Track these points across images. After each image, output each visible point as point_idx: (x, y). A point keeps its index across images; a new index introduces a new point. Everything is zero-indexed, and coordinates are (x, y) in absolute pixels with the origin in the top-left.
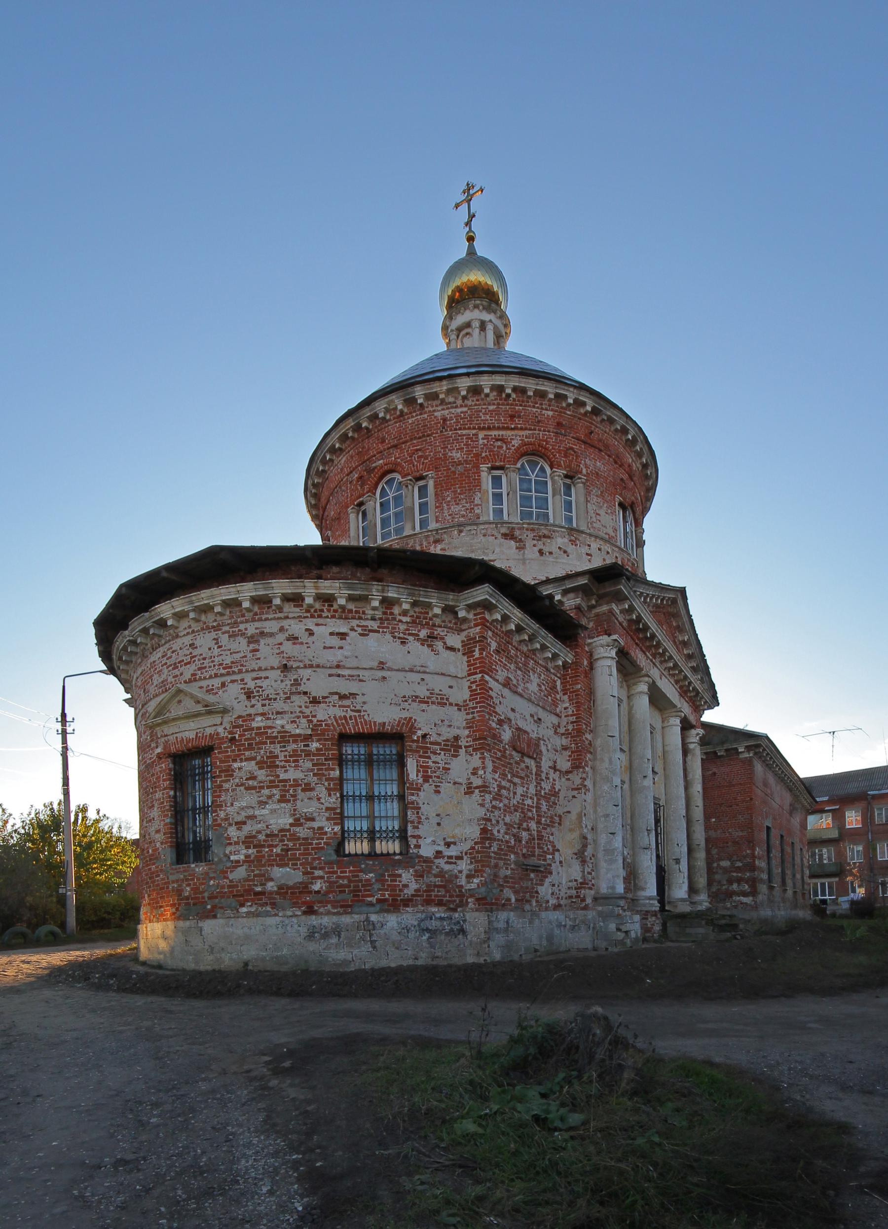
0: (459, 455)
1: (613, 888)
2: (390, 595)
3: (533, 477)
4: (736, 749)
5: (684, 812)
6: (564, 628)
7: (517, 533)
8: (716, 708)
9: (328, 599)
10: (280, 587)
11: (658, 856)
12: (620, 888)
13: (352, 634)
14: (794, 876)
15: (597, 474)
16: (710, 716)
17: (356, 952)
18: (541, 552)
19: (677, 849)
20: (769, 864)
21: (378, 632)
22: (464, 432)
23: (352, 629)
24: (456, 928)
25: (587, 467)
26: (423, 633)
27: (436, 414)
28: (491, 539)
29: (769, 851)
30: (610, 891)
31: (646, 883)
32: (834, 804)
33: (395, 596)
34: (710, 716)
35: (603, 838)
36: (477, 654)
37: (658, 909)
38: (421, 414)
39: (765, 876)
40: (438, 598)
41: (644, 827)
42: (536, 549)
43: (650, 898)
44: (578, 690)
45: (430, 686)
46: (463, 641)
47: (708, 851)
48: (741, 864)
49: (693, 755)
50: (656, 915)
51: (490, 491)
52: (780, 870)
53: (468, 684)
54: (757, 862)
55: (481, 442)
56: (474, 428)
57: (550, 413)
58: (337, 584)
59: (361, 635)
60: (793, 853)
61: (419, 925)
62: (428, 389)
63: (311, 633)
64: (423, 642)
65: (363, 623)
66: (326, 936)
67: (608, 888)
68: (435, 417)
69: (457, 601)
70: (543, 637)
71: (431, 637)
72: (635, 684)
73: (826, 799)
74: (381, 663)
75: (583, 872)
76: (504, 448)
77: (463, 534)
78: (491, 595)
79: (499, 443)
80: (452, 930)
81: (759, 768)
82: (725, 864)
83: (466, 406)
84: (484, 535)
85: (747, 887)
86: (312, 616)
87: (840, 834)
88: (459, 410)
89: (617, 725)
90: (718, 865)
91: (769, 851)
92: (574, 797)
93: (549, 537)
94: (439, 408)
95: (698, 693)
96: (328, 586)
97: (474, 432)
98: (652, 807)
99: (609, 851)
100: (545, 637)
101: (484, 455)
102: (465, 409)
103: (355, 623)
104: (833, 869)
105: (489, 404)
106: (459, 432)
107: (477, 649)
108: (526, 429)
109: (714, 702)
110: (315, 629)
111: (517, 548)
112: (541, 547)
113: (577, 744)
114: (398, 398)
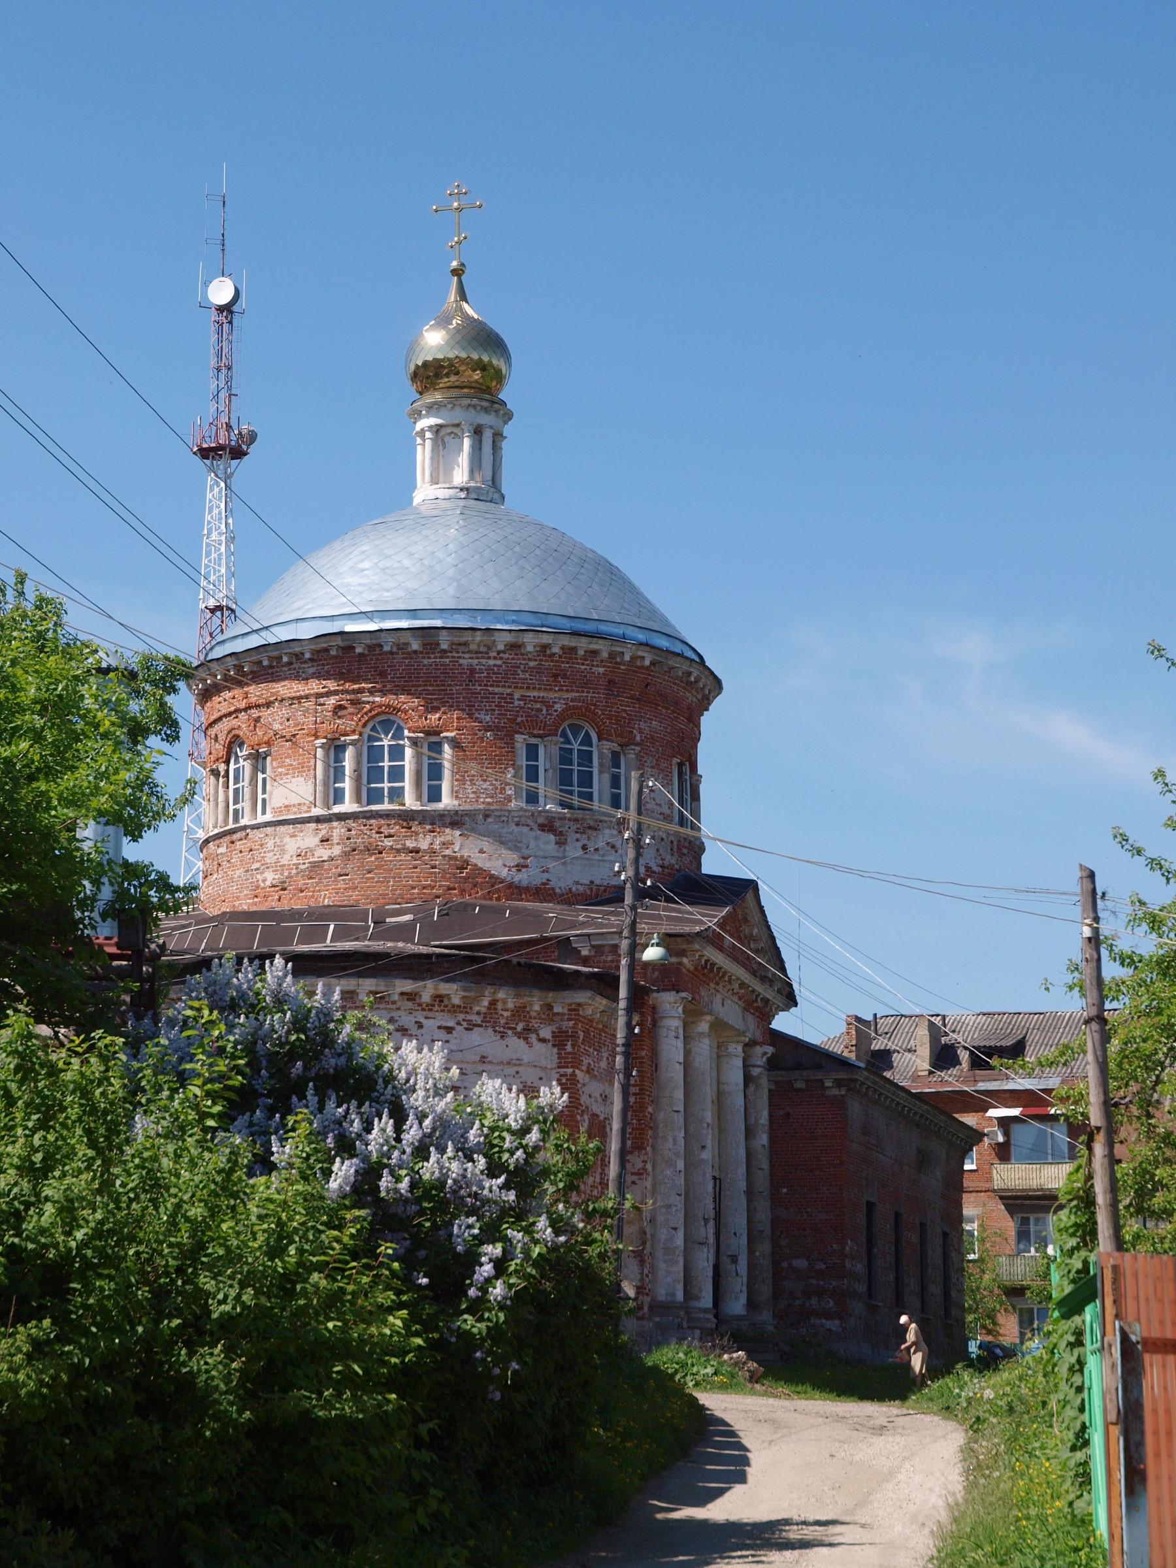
0: (488, 718)
1: (673, 1295)
3: (576, 746)
4: (822, 1081)
5: (743, 1185)
7: (557, 824)
9: (439, 998)
12: (680, 1296)
13: (459, 1028)
14: (923, 1289)
15: (652, 737)
18: (584, 848)
20: (870, 1266)
21: (480, 1026)
22: (496, 690)
23: (459, 1023)
25: (641, 731)
26: (520, 1027)
27: (461, 661)
28: (525, 830)
29: (870, 1243)
30: (669, 1298)
31: (700, 1290)
34: (783, 1022)
35: (663, 1234)
36: (569, 1048)
38: (441, 657)
39: (861, 1288)
41: (700, 1215)
42: (579, 844)
43: (705, 1311)
44: (643, 1058)
45: (523, 1079)
46: (553, 1032)
47: (775, 1240)
48: (823, 1266)
51: (525, 763)
52: (892, 1276)
53: (557, 1076)
54: (848, 1265)
55: (517, 703)
56: (510, 687)
57: (601, 670)
58: (454, 986)
59: (466, 1029)
60: (923, 1245)
63: (420, 1026)
64: (519, 1035)
65: (469, 1017)
67: (667, 1295)
68: (460, 665)
71: (527, 1030)
74: (483, 1057)
75: (642, 1274)
76: (544, 712)
77: (490, 820)
79: (538, 706)
81: (855, 1108)
82: (801, 1263)
83: (501, 658)
84: (517, 825)
85: (832, 1303)
86: (423, 1010)
88: (492, 662)
90: (790, 1264)
91: (870, 1243)
92: (634, 1183)
93: (596, 829)
94: (467, 656)
95: (768, 1001)
96: (446, 988)
97: (509, 691)
99: (669, 1250)
101: (519, 720)
102: (499, 662)
103: (461, 1017)
105: (530, 660)
106: (491, 689)
107: (569, 1043)
108: (572, 691)
109: (790, 999)
110: (425, 1022)
111: (557, 843)
112: (585, 842)
113: (639, 1120)
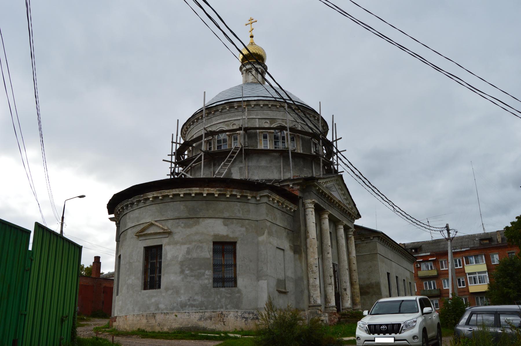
5: (347, 267)
10: (195, 190)
11: (336, 287)
16: (357, 222)
17: (217, 326)
19: (344, 284)
31: (330, 300)
32: (433, 257)
34: (357, 222)
43: (332, 307)
49: (351, 240)
50: (335, 314)
58: (215, 189)
66: (206, 319)
73: (429, 254)
80: (253, 318)
87: (438, 273)
89: (319, 283)
98: (332, 266)
100: (287, 203)
104: (436, 293)
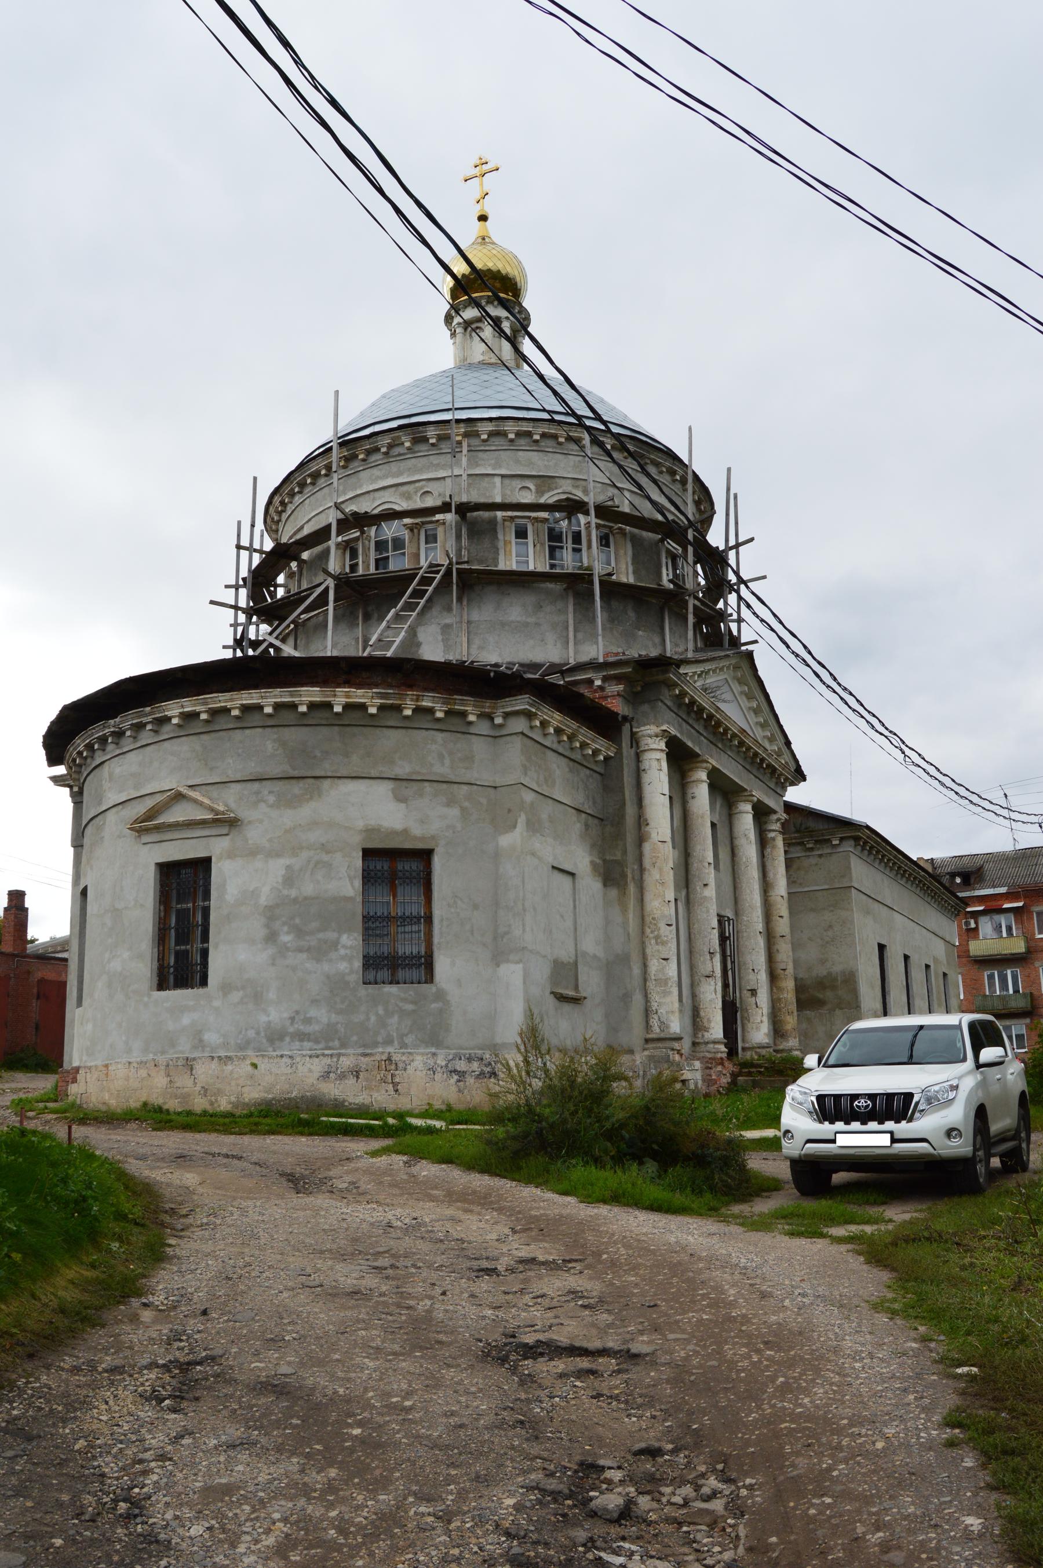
2: (424, 704)
6: (606, 724)
8: (802, 783)
10: (309, 694)
11: (725, 986)
16: (794, 795)
17: (375, 1095)
24: (487, 1069)
31: (709, 1021)
33: (430, 704)
34: (794, 795)
37: (724, 1055)
40: (474, 706)
41: (706, 950)
50: (722, 1064)
58: (370, 692)
61: (447, 1066)
62: (442, 430)
66: (342, 1077)
69: (494, 708)
70: (583, 735)
72: (691, 770)
73: (1003, 890)
78: (531, 705)
80: (482, 1073)
96: (359, 695)
100: (585, 734)
104: (1021, 1004)
114: (405, 435)
